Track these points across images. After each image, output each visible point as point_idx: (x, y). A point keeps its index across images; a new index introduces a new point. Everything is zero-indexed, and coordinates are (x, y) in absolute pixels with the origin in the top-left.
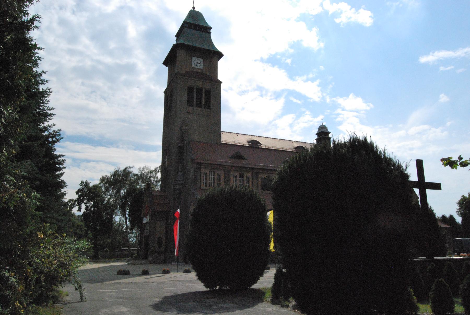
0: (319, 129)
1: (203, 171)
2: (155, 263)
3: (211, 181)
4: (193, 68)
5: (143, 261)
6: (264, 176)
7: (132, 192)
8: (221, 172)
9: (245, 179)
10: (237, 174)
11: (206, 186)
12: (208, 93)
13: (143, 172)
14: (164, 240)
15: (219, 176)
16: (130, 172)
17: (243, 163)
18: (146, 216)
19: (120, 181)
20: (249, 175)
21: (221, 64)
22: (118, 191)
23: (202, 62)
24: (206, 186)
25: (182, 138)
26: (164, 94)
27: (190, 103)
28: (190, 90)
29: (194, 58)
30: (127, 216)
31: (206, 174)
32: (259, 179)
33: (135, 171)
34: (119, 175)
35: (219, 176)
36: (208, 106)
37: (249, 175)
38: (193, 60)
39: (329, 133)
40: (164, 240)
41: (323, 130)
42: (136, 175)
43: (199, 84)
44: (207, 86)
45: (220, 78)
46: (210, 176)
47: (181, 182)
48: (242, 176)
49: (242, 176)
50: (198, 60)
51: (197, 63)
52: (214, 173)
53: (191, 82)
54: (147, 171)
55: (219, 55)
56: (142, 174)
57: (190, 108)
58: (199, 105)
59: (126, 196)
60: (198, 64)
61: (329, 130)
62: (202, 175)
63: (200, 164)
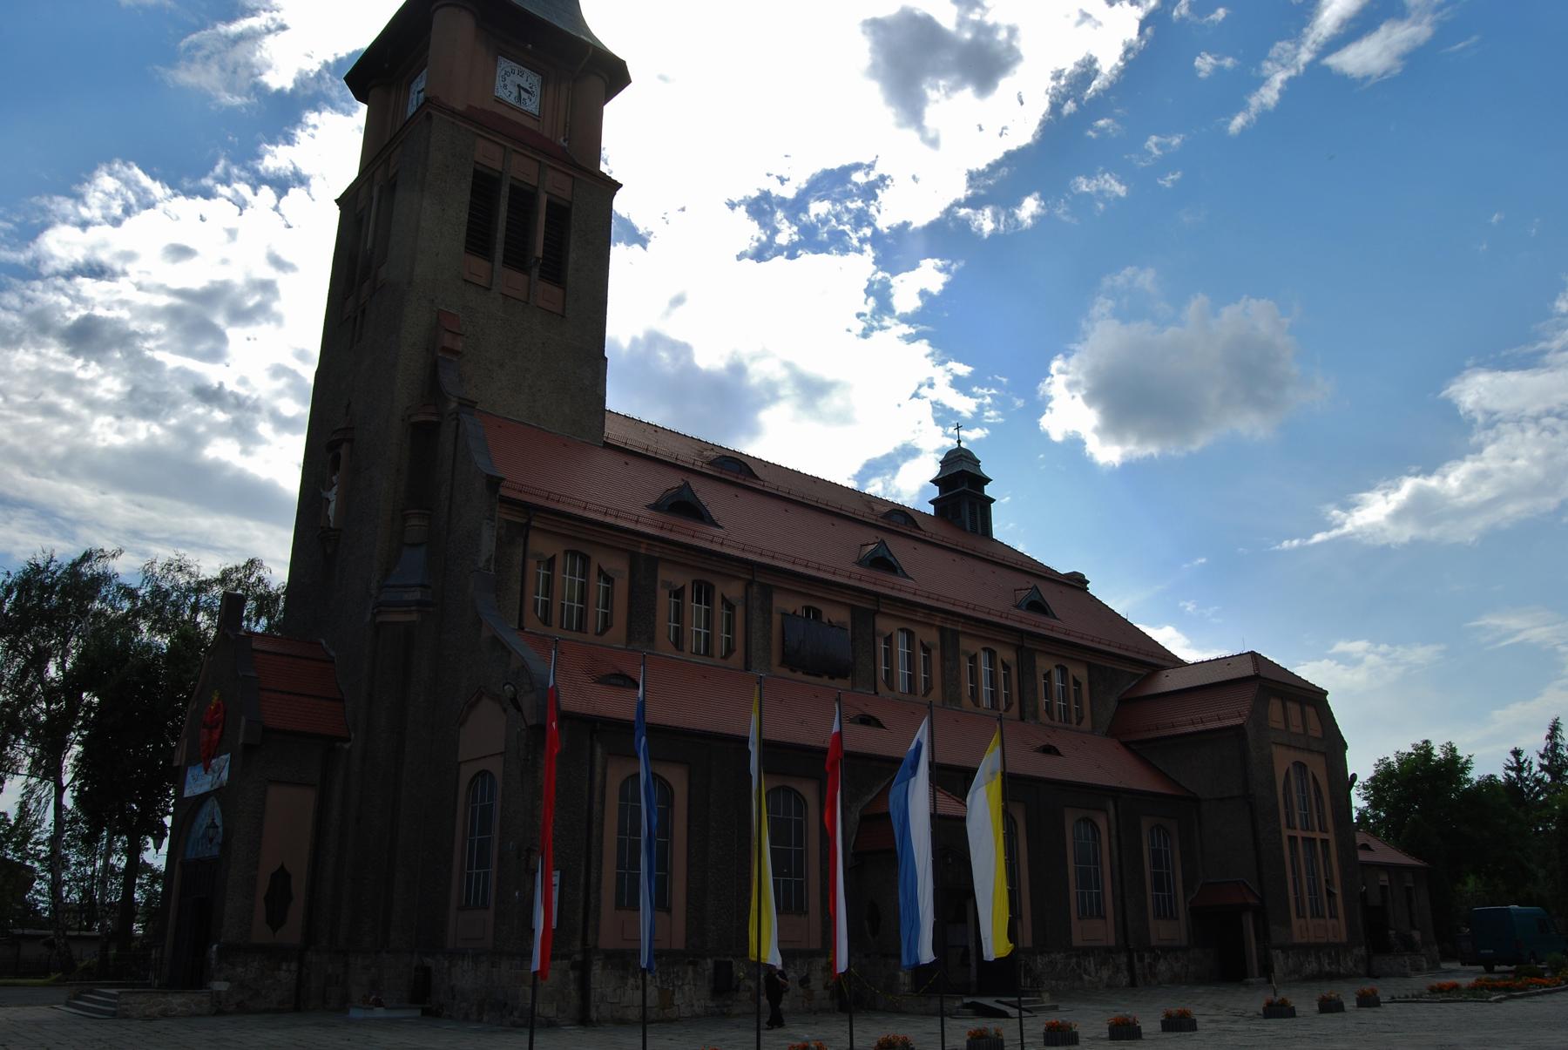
0: (945, 463)
1: (542, 545)
2: (242, 1009)
3: (571, 600)
4: (499, 101)
5: (177, 1001)
6: (794, 605)
7: (110, 659)
8: (618, 566)
9: (720, 611)
10: (682, 579)
11: (546, 620)
12: (559, 215)
13: (166, 585)
14: (299, 887)
15: (609, 580)
16: (103, 579)
17: (702, 537)
18: (204, 760)
19: (49, 617)
20: (734, 590)
21: (615, 114)
22: (38, 661)
23: (537, 90)
24: (546, 620)
25: (433, 389)
26: (335, 213)
27: (478, 242)
28: (484, 186)
29: (505, 65)
30: (67, 778)
31: (550, 563)
32: (776, 618)
33: (126, 567)
34: (47, 589)
35: (609, 580)
36: (554, 270)
37: (734, 590)
38: (500, 72)
39: (988, 480)
40: (299, 887)
41: (966, 467)
42: (130, 593)
43: (522, 169)
44: (553, 185)
45: (612, 162)
46: (567, 580)
47: (416, 595)
48: (704, 592)
49: (704, 592)
50: (521, 74)
51: (514, 87)
52: (586, 560)
53: (489, 154)
54: (182, 580)
55: (614, 75)
56: (157, 592)
57: (478, 264)
58: (517, 258)
59: (72, 684)
60: (524, 95)
61: (985, 469)
62: (532, 563)
63: (527, 508)
